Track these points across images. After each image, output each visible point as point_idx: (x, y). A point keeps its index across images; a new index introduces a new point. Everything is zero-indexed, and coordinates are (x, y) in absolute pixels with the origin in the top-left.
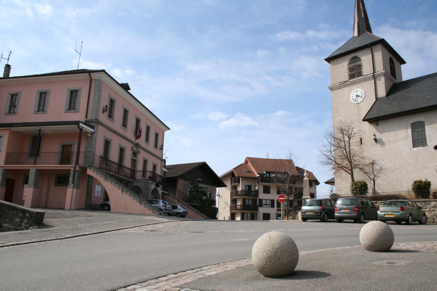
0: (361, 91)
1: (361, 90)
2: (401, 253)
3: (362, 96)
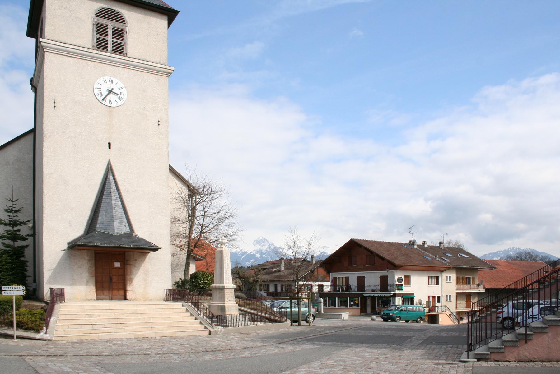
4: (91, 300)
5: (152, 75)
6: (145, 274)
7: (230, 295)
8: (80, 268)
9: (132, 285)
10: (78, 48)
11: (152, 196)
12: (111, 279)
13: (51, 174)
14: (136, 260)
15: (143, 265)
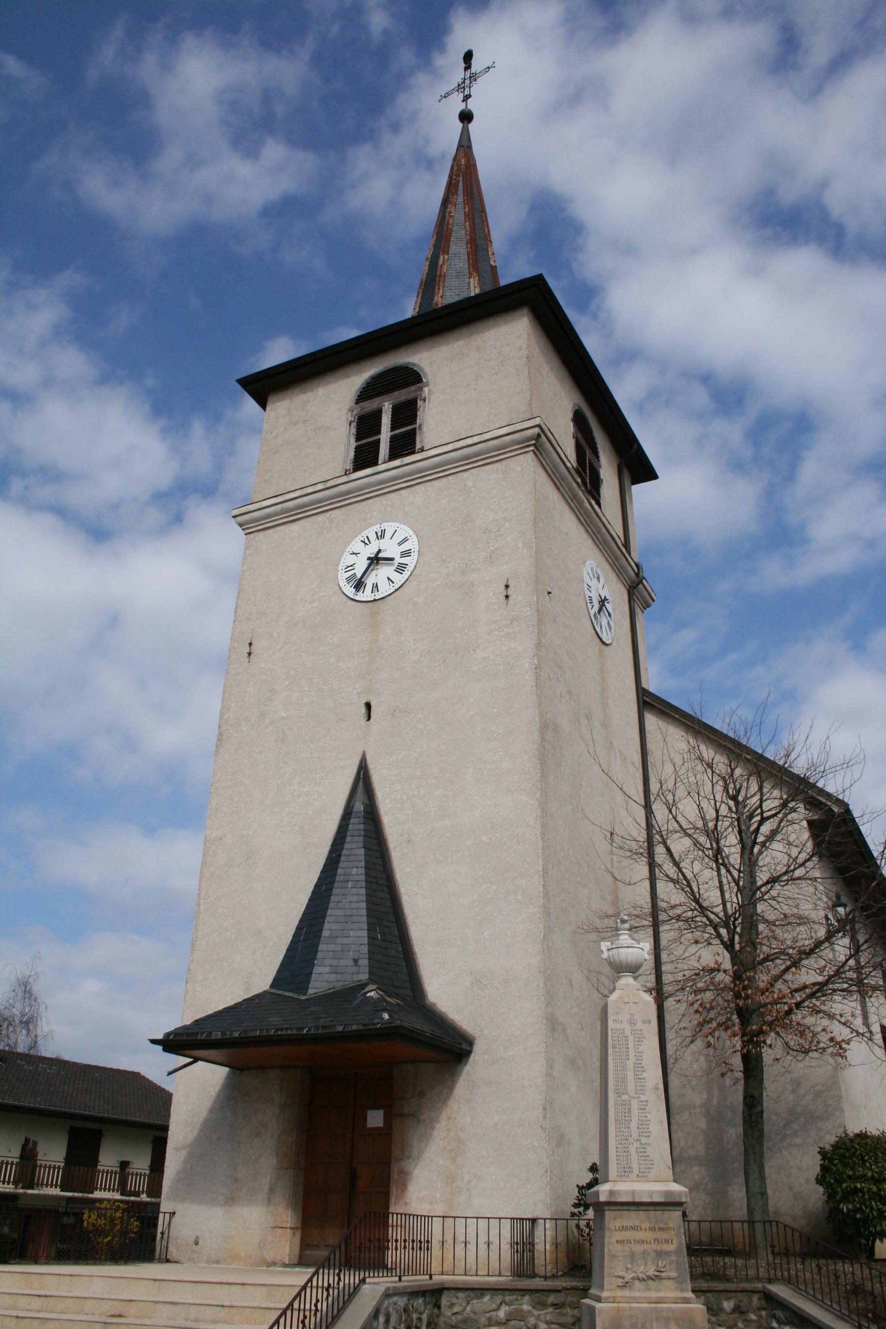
0: (399, 537)
1: (404, 531)
2: (398, 392)
3: (404, 560)
4: (274, 1264)
5: (487, 468)
6: (451, 1150)
7: (654, 1246)
8: (256, 1136)
9: (406, 1204)
10: (304, 491)
11: (483, 838)
12: (353, 1178)
13: (221, 838)
14: (422, 1094)
15: (444, 1115)
